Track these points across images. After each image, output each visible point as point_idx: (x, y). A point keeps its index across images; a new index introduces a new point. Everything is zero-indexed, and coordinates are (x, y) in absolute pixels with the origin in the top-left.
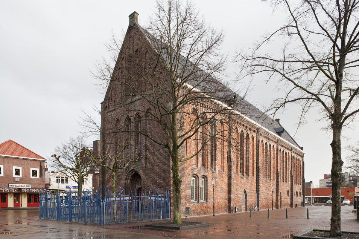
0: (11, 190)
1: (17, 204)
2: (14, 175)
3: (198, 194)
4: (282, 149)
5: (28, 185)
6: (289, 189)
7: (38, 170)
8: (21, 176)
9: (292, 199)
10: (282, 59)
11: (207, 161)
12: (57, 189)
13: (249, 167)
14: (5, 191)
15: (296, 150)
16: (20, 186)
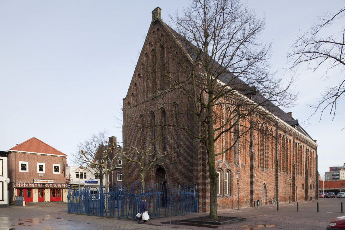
0: (36, 185)
1: (41, 199)
2: (38, 171)
3: (223, 188)
4: (298, 142)
5: (51, 180)
6: (304, 182)
7: (59, 166)
8: (44, 172)
9: (306, 192)
10: (342, 43)
11: (231, 155)
12: (78, 183)
13: (268, 161)
14: (30, 186)
15: (310, 143)
16: (43, 182)
